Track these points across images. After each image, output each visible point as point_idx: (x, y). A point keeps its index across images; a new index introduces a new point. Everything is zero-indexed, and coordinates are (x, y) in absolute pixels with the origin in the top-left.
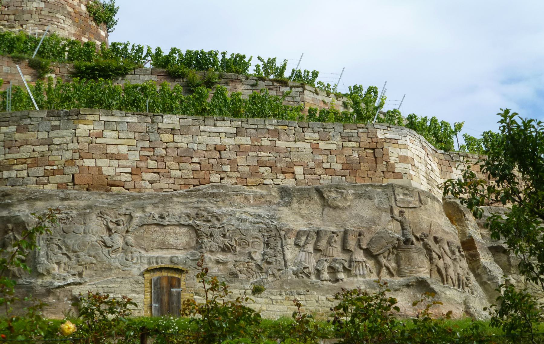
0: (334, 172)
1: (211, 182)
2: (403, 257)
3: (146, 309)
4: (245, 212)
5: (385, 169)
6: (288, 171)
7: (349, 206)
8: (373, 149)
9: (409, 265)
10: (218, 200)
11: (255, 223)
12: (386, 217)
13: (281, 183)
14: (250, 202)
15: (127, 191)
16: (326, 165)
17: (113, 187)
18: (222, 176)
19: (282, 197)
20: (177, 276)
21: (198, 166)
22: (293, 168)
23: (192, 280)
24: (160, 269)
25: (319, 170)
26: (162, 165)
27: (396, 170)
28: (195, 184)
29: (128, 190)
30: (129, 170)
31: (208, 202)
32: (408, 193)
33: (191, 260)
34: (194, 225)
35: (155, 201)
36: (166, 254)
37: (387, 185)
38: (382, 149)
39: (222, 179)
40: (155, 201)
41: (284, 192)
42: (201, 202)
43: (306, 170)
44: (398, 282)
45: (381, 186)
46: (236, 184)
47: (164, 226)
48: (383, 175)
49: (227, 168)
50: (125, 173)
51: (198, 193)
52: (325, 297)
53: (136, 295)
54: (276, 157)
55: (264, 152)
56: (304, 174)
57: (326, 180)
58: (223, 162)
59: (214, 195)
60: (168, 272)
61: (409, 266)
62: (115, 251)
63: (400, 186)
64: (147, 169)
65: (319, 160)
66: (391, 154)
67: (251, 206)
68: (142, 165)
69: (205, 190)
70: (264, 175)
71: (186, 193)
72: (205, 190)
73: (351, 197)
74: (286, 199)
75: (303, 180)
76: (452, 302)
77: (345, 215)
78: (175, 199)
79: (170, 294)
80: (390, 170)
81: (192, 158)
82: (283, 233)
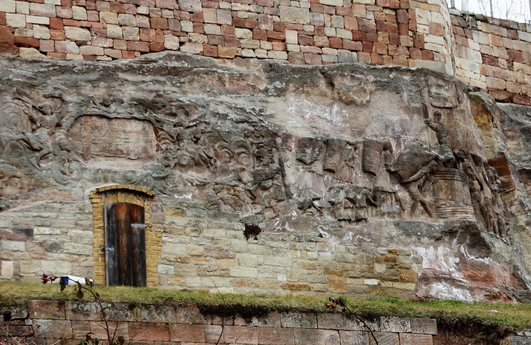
0: (336, 44)
1: (166, 49)
2: (443, 187)
3: (96, 255)
4: (222, 103)
5: (411, 44)
6: (276, 36)
7: (368, 102)
8: (395, 10)
9: (451, 200)
10: (182, 80)
11: (238, 122)
12: (418, 122)
13: (266, 56)
14: (225, 85)
15: (44, 56)
16: (330, 32)
17: (22, 49)
18: (182, 39)
19: (271, 80)
20: (138, 202)
21: (147, 19)
22: (284, 33)
23: (159, 212)
24: (114, 191)
25: (320, 39)
26: (93, 16)
27: (426, 47)
28: (143, 50)
29: (45, 53)
30: (47, 21)
31: (169, 83)
32: (443, 84)
33: (155, 178)
34: (152, 119)
35: (93, 76)
36: (112, 166)
37: (417, 70)
38: (407, 10)
39: (181, 44)
40: (93, 76)
41: (272, 69)
42: (158, 82)
43: (307, 39)
44: (439, 226)
45: (409, 71)
46: (202, 53)
47: (109, 119)
48: (407, 52)
49: (187, 26)
50: (39, 25)
51: (151, 65)
52: (38, 238)
53: (82, 232)
54: (258, 13)
55: (242, 4)
56: (299, 44)
57: (330, 55)
58: (182, 16)
59: (174, 72)
60: (135, 198)
61: (452, 202)
62: (44, 157)
63: (433, 72)
64: (73, 21)
65: (320, 22)
66: (418, 20)
67: (228, 92)
68: (64, 13)
69: (161, 62)
70: (241, 41)
71: (135, 65)
72: (161, 62)
73: (371, 87)
74: (278, 84)
75: (298, 53)
76: (499, 259)
77: (362, 116)
78: (121, 75)
79: (130, 231)
80: (418, 45)
81: (137, 6)
82: (279, 141)
